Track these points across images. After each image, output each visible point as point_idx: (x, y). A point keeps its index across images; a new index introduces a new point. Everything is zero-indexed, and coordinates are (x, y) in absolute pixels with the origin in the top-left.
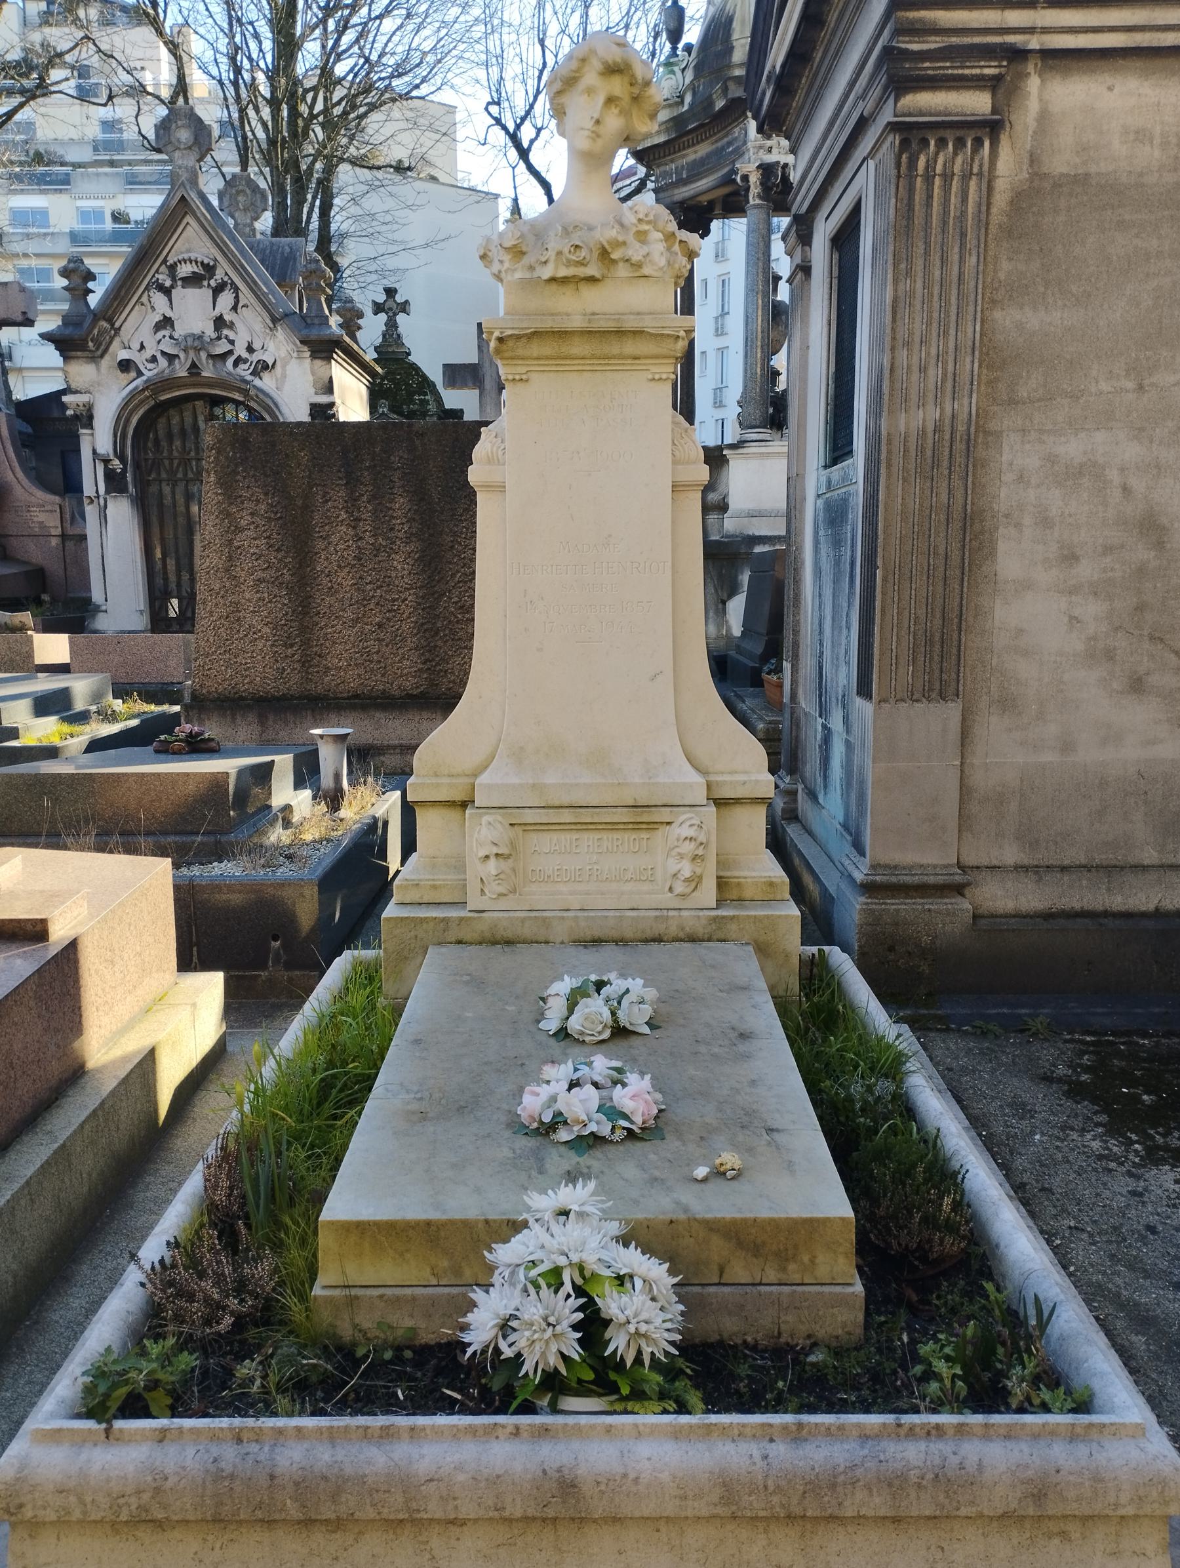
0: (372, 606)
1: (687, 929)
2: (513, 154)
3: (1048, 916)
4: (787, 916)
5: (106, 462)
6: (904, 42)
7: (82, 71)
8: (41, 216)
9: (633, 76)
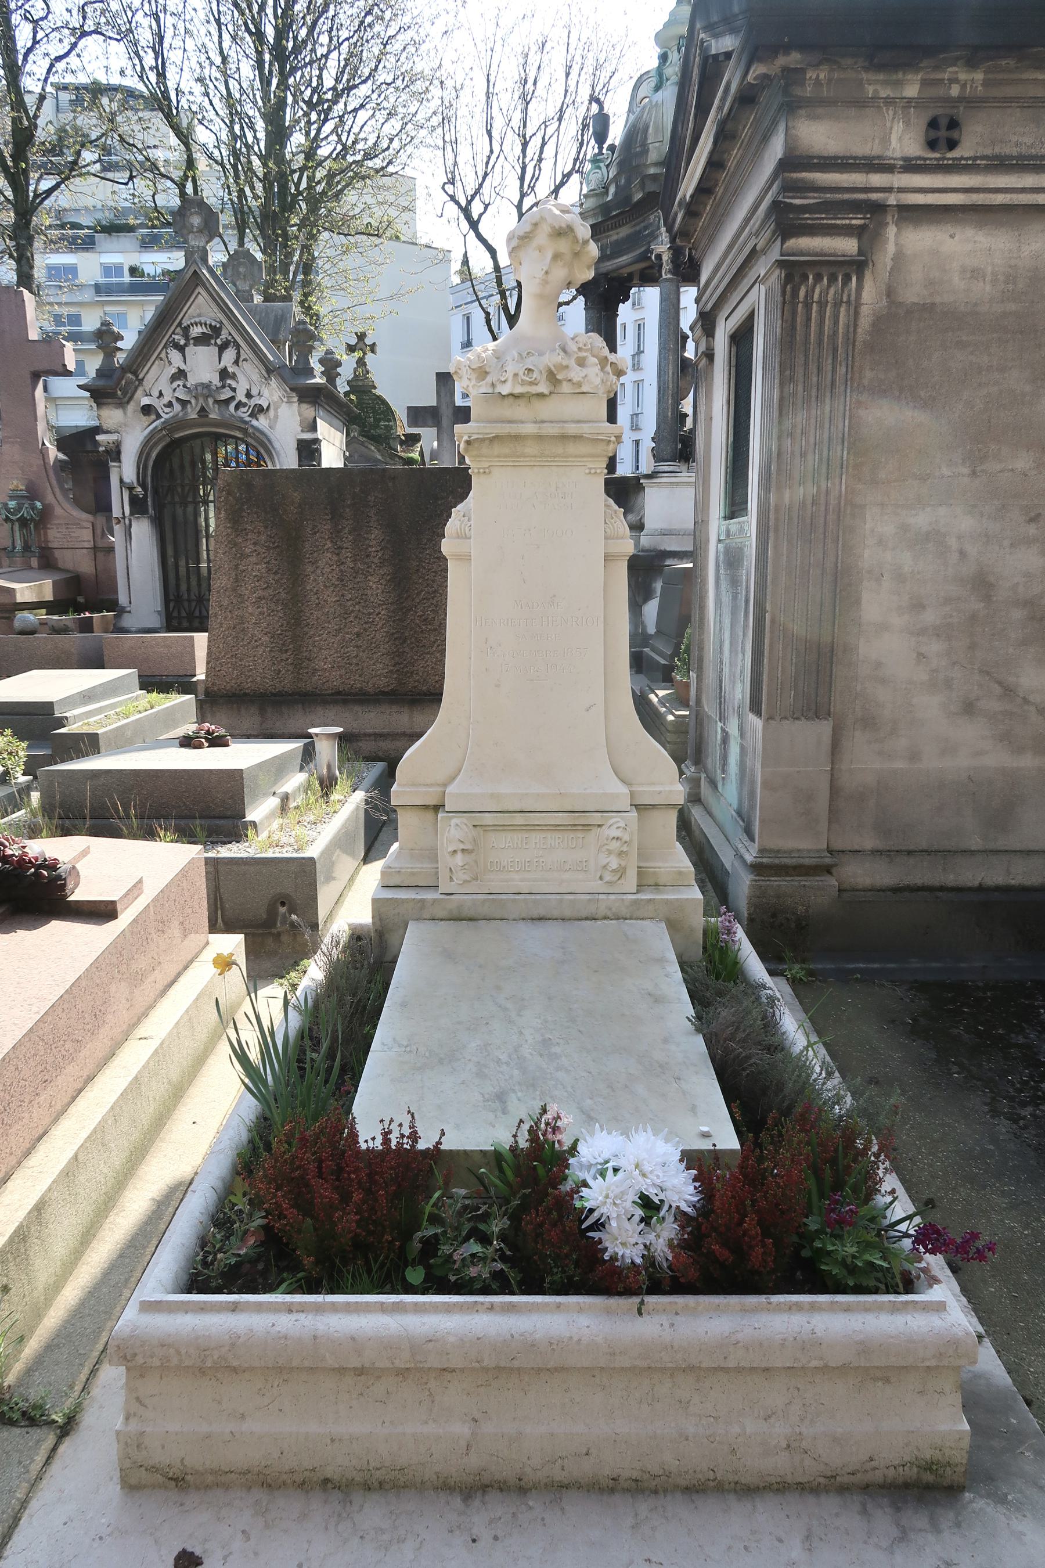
0: (351, 619)
1: (614, 909)
2: (465, 225)
3: (896, 890)
4: (693, 899)
5: (131, 489)
6: (789, 198)
7: (107, 150)
8: (72, 270)
9: (575, 237)
